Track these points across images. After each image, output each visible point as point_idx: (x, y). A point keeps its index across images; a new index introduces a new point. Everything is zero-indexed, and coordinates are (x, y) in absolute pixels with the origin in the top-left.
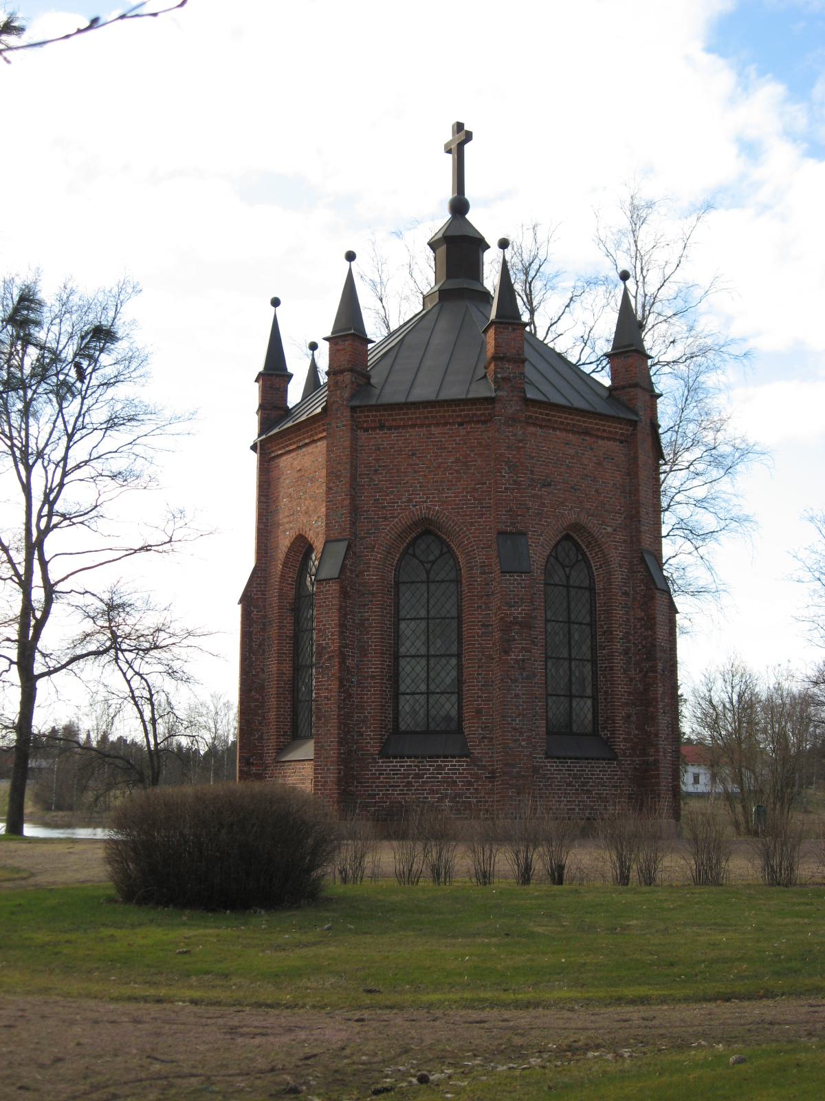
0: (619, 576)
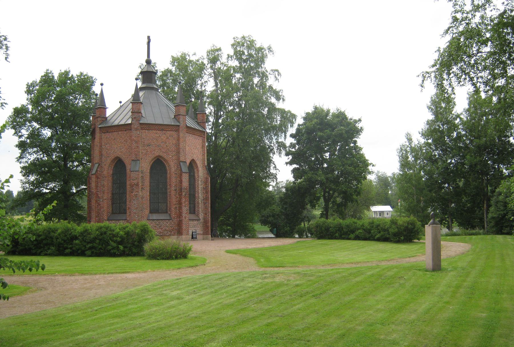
0: (173, 170)
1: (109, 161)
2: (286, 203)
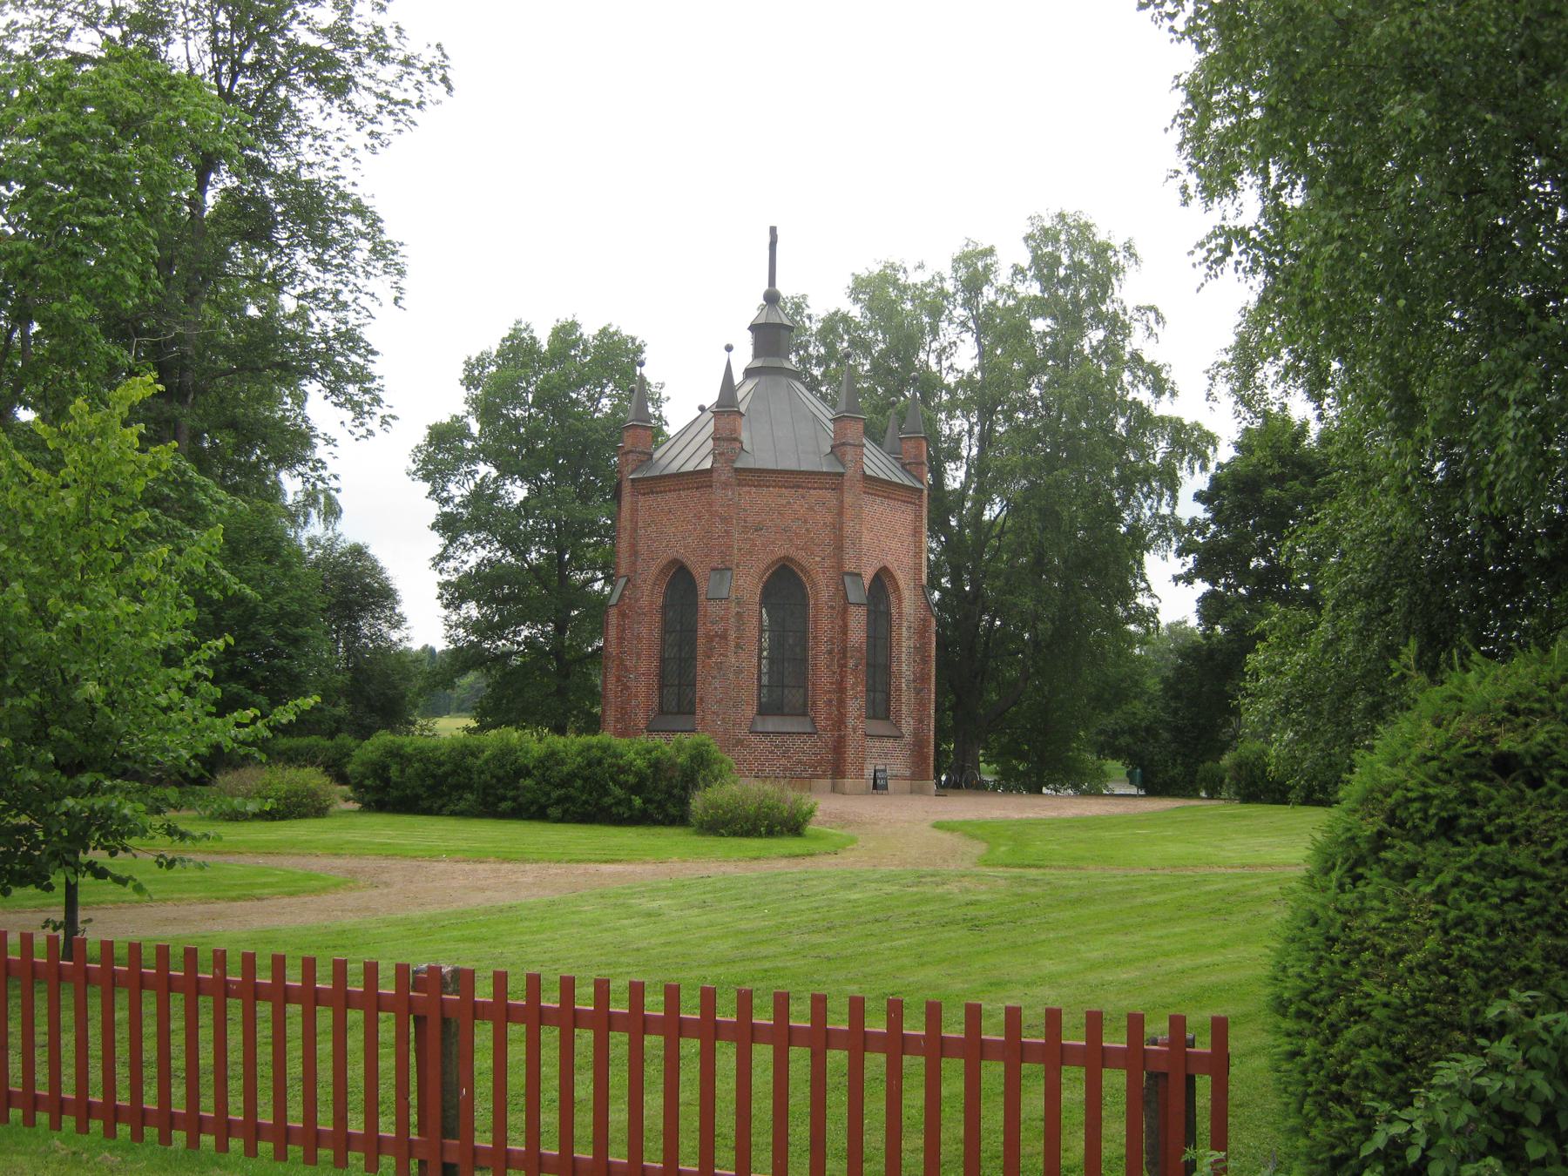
1: (654, 569)
2: (1177, 697)
